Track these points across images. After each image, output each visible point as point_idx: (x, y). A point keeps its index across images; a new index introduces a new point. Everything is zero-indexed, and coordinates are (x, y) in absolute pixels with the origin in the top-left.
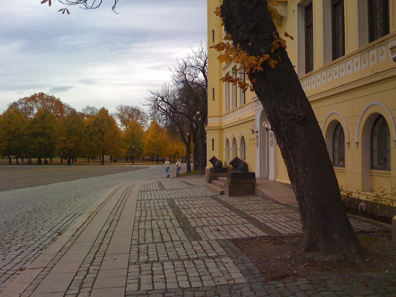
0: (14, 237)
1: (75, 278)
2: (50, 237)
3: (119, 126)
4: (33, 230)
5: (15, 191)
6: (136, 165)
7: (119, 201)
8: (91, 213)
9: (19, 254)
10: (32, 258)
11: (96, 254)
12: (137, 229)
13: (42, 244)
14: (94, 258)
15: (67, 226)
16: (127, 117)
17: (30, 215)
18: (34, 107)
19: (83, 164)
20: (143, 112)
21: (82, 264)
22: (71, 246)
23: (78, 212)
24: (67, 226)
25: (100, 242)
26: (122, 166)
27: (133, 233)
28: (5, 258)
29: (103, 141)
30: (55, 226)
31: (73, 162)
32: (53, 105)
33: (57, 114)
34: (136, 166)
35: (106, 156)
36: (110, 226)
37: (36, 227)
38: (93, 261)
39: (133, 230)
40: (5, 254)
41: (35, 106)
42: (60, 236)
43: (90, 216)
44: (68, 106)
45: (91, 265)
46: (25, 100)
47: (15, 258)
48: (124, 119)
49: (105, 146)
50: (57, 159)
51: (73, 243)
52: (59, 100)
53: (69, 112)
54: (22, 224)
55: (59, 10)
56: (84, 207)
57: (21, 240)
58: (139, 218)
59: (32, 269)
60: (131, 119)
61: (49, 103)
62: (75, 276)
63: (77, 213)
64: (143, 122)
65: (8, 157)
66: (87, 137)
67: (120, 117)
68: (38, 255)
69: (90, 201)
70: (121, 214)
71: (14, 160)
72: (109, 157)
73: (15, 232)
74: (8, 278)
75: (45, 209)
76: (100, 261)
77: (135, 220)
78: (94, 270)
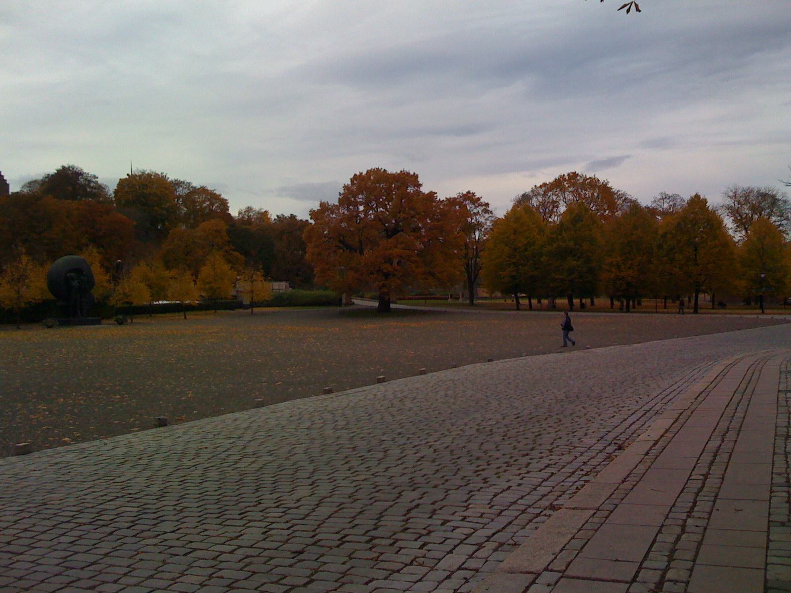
0: (534, 445)
1: (657, 538)
2: (601, 451)
3: (731, 232)
4: (568, 434)
5: (529, 358)
6: (770, 314)
7: (738, 390)
8: (680, 411)
9: (545, 478)
10: (571, 488)
11: (697, 494)
12: (782, 451)
13: (588, 463)
14: (695, 503)
15: (633, 434)
16: (747, 212)
17: (562, 405)
18: (560, 200)
19: (655, 310)
20: (784, 199)
21: (670, 511)
22: (644, 474)
23: (653, 407)
24: (633, 434)
25: (704, 472)
26: (739, 316)
27: (773, 461)
28: (521, 482)
29: (697, 265)
30: (609, 432)
31: (634, 307)
32: (596, 194)
33: (602, 212)
34: (769, 317)
35: (703, 295)
36: (723, 441)
37: (574, 430)
38: (692, 508)
39: (774, 453)
40: (522, 475)
41: (562, 198)
42: (620, 451)
43: (679, 417)
44: (623, 194)
45: (688, 517)
46: (544, 188)
47: (540, 485)
48: (740, 216)
49: (700, 274)
50: (602, 301)
51: (649, 467)
52: (606, 184)
53: (626, 207)
54: (547, 421)
55: (619, 8)
56: (663, 398)
57: (548, 453)
58: (785, 429)
59: (574, 509)
60: (756, 216)
61: (587, 191)
62: (657, 535)
63: (650, 409)
64: (784, 222)
65: (513, 296)
66: (664, 257)
67: (731, 213)
68: (583, 483)
69: (674, 387)
70: (744, 418)
71: (524, 302)
72: (708, 297)
73: (536, 436)
74: (530, 521)
75: (588, 397)
76: (708, 509)
77: (776, 433)
78: (696, 526)
